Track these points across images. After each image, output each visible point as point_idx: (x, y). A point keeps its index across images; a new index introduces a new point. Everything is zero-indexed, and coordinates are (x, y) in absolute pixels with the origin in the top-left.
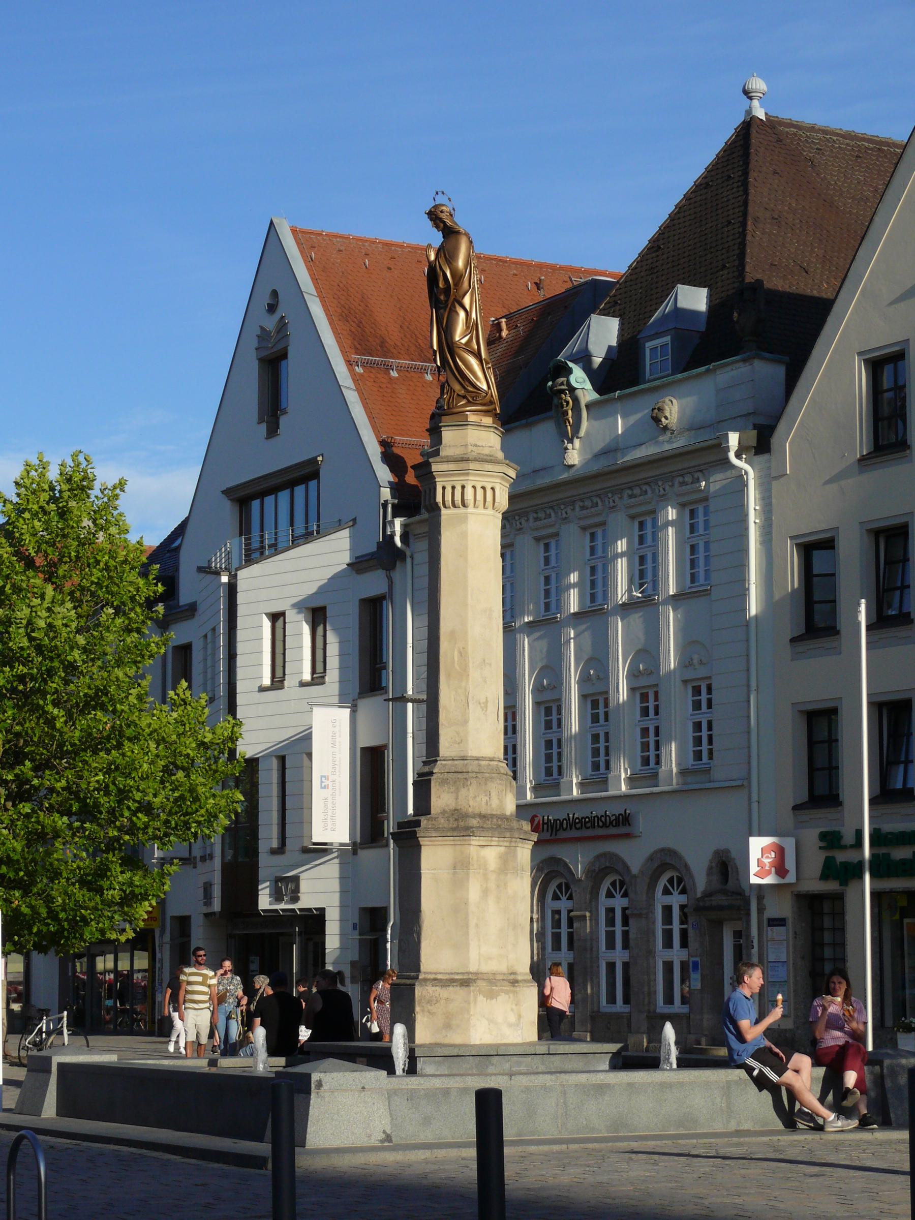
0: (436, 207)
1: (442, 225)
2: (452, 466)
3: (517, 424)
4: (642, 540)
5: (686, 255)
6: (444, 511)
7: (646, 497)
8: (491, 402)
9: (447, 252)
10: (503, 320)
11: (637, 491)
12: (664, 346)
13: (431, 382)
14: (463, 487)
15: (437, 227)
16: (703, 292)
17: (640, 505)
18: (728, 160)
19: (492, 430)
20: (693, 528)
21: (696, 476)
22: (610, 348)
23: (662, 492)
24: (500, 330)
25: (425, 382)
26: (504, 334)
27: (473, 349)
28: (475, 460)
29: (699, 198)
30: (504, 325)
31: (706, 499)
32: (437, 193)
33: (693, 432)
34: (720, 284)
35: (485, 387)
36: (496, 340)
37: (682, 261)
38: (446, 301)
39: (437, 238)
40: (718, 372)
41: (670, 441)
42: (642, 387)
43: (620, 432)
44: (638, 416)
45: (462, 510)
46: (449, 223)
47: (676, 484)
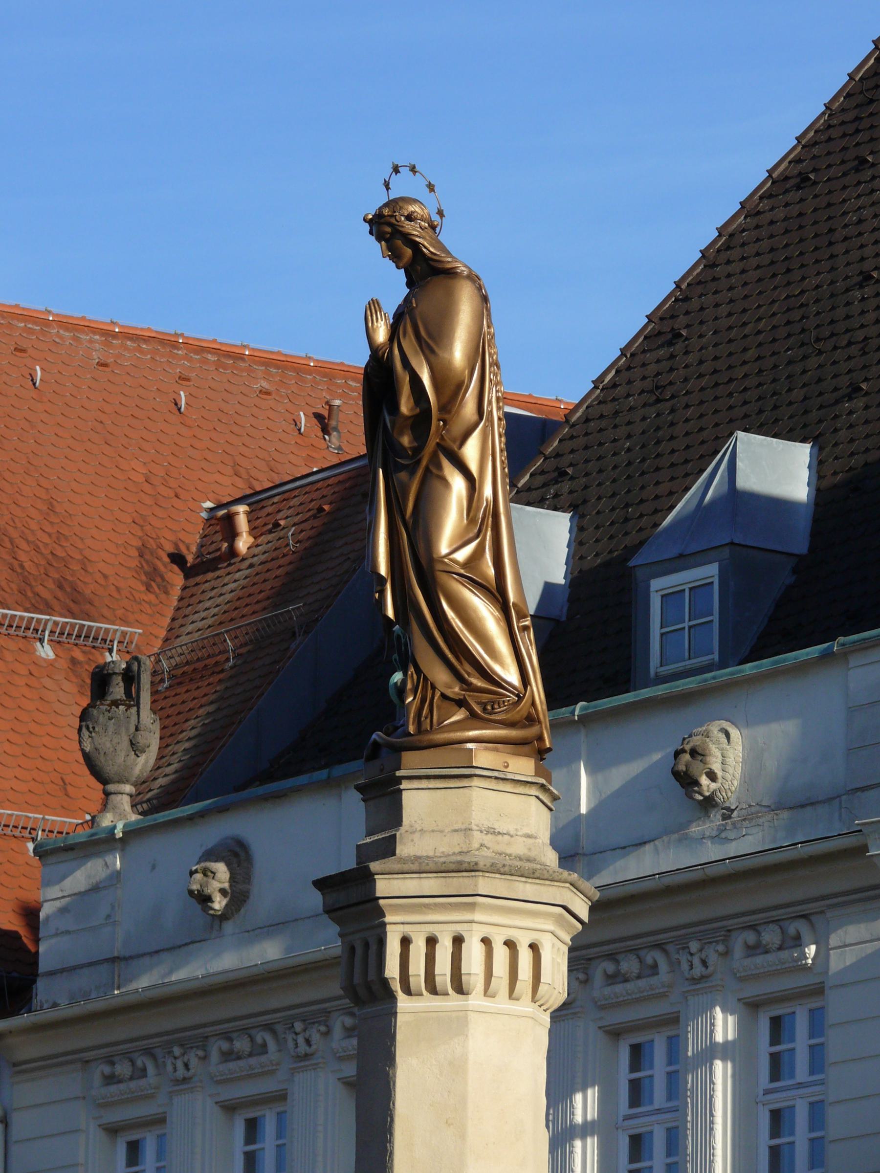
2: (430, 884)
3: (303, 779)
4: (637, 1092)
5: (751, 354)
6: (403, 1003)
8: (531, 720)
11: (629, 965)
12: (699, 590)
13: (51, 663)
14: (458, 941)
15: (395, 256)
16: (801, 454)
17: (638, 1000)
18: (858, 119)
19: (534, 791)
20: (778, 1066)
21: (792, 930)
22: (549, 588)
24: (232, 534)
25: (37, 662)
26: (243, 543)
27: (484, 576)
29: (780, 213)
30: (242, 522)
31: (819, 990)
32: (396, 170)
33: (785, 815)
34: (843, 434)
35: (512, 676)
37: (739, 372)
38: (418, 450)
40: (853, 661)
41: (719, 837)
42: (645, 693)
43: (583, 810)
45: (454, 1001)
46: (429, 248)
47: (738, 950)
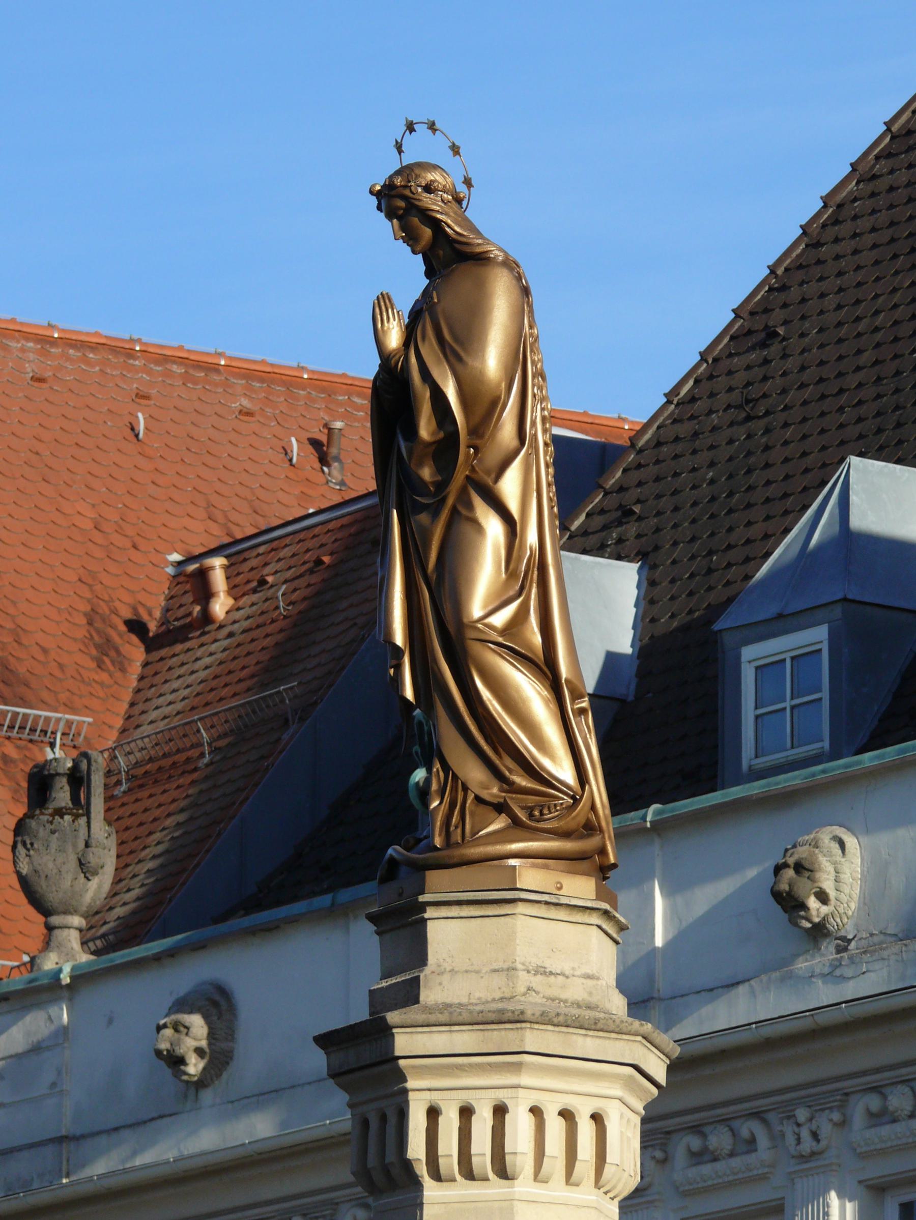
0: (407, 171)
1: (427, 232)
2: (464, 1040)
5: (867, 357)
6: (431, 1191)
7: (752, 1159)
8: (590, 828)
9: (441, 322)
10: (218, 562)
14: (500, 1111)
15: (410, 238)
17: (730, 1185)
19: (595, 919)
22: (612, 659)
23: (808, 1144)
24: (205, 594)
26: (220, 606)
28: (546, 1020)
30: (219, 579)
32: (411, 127)
35: (565, 772)
36: (190, 627)
37: (852, 381)
38: (442, 486)
39: (407, 276)
41: (832, 975)
43: (659, 942)
44: (725, 887)
45: (495, 1188)
46: (453, 227)
